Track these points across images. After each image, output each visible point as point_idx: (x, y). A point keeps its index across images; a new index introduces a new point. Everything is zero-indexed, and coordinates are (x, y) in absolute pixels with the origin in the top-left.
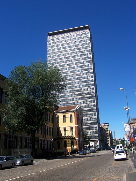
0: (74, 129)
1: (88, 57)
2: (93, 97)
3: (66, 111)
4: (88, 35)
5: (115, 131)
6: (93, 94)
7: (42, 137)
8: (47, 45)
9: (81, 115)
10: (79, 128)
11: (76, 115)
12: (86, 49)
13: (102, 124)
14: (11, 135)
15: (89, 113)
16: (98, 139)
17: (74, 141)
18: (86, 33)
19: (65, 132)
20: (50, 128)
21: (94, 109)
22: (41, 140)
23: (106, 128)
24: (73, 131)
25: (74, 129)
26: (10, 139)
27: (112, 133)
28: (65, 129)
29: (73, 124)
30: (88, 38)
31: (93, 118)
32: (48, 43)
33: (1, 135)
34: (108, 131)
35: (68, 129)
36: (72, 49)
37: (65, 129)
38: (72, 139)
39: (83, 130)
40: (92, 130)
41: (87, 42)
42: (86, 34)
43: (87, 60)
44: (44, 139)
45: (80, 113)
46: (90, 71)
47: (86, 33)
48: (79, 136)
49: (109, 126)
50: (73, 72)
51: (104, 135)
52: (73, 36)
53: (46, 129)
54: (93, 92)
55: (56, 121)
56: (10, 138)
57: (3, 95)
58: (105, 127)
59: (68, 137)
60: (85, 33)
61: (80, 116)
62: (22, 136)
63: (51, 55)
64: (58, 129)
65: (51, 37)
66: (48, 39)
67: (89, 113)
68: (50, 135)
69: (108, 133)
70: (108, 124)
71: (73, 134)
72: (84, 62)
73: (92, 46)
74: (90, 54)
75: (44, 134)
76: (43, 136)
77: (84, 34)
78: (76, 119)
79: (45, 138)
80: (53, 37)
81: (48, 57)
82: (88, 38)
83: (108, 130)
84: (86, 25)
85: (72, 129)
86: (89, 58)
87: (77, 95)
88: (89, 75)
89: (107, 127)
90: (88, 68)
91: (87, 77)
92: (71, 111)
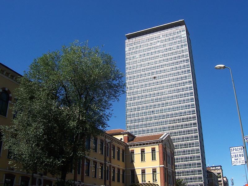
0: (158, 171)
1: (184, 66)
2: (195, 124)
3: (145, 142)
4: (184, 34)
5: (233, 178)
6: (195, 126)
8: (125, 51)
9: (170, 149)
10: (167, 170)
11: (161, 148)
13: (211, 167)
15: (188, 148)
19: (143, 177)
20: (119, 170)
21: (197, 143)
23: (217, 173)
24: (157, 175)
25: (158, 171)
27: (228, 181)
28: (143, 172)
29: (157, 164)
31: (194, 157)
33: (15, 176)
34: (220, 177)
35: (149, 172)
36: (161, 55)
37: (143, 172)
39: (176, 176)
40: (194, 174)
41: (183, 43)
42: (181, 32)
45: (168, 146)
46: (188, 86)
48: (166, 184)
49: (222, 170)
52: (162, 37)
54: (194, 117)
55: (128, 158)
57: (10, 102)
58: (215, 172)
60: (178, 31)
61: (168, 151)
63: (131, 66)
64: (133, 171)
65: (131, 40)
67: (189, 148)
68: (119, 181)
69: (221, 181)
70: (221, 166)
71: (156, 180)
72: (178, 73)
73: (191, 55)
74: (187, 60)
77: (178, 32)
78: (161, 154)
81: (127, 68)
83: (222, 175)
84: (180, 19)
85: (154, 171)
88: (183, 54)
89: (219, 172)
90: (185, 81)
92: (154, 143)
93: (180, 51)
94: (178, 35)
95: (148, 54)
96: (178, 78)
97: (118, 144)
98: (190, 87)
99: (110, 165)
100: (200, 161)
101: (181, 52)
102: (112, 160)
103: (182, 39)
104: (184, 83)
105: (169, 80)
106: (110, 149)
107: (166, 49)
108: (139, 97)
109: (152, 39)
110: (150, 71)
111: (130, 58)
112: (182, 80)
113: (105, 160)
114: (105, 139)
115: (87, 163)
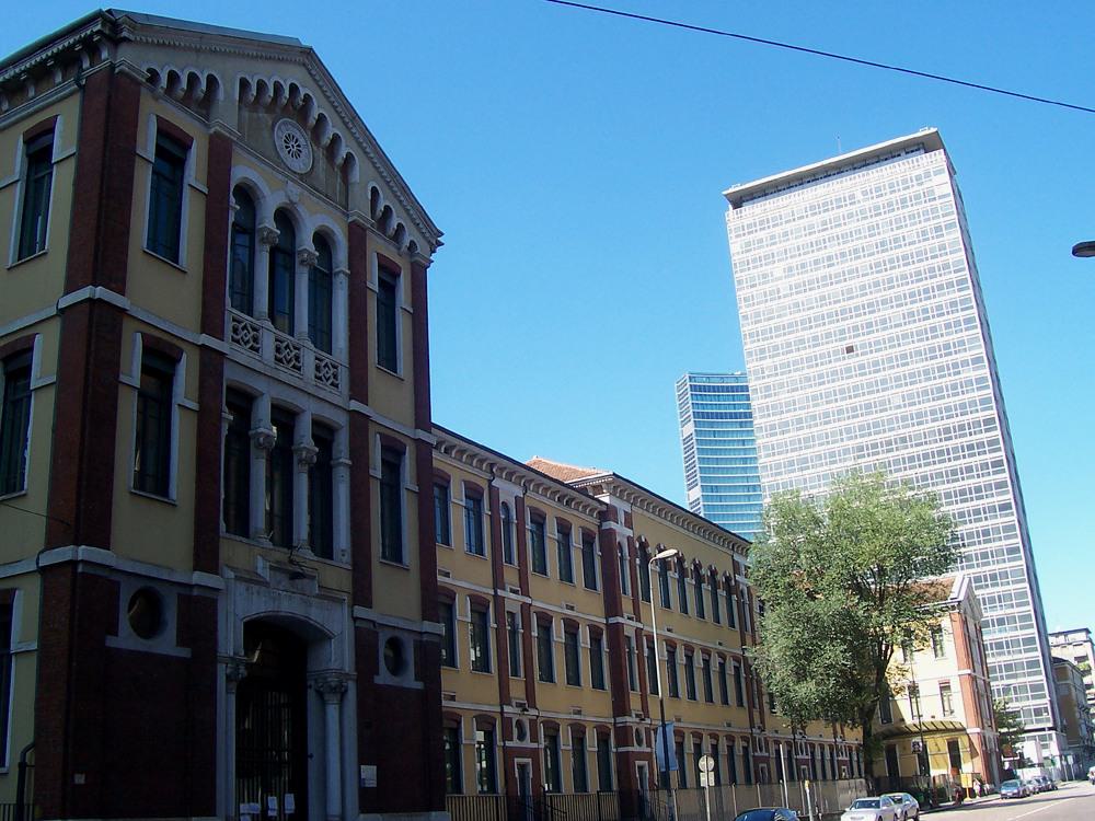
1: (953, 304)
6: (1014, 559)
7: (748, 724)
12: (939, 259)
14: (511, 719)
16: (1050, 725)
17: (963, 742)
18: (927, 175)
19: (914, 705)
20: (572, 628)
22: (485, 722)
25: (955, 685)
26: (512, 740)
30: (940, 197)
31: (1012, 619)
32: (735, 246)
38: (953, 733)
43: (951, 316)
44: (839, 740)
47: (927, 175)
50: (887, 389)
51: (1074, 697)
53: (527, 637)
56: (507, 736)
57: (668, 573)
59: (932, 727)
62: (732, 729)
66: (731, 226)
72: (933, 329)
75: (752, 705)
76: (835, 730)
77: (918, 178)
79: (759, 728)
80: (752, 211)
82: (940, 197)
85: (945, 687)
86: (963, 327)
87: (829, 397)
89: (1080, 651)
91: (963, 406)
93: (932, 250)
94: (920, 188)
95: (816, 262)
96: (932, 350)
97: (583, 516)
98: (979, 380)
99: (525, 608)
100: (1006, 476)
101: (938, 253)
102: (534, 581)
103: (938, 202)
104: (955, 365)
105: (904, 356)
106: (517, 525)
107: (883, 244)
108: (800, 421)
109: (825, 204)
110: (832, 327)
111: (753, 279)
112: (950, 354)
113: (498, 582)
114: (490, 481)
115: (476, 615)
